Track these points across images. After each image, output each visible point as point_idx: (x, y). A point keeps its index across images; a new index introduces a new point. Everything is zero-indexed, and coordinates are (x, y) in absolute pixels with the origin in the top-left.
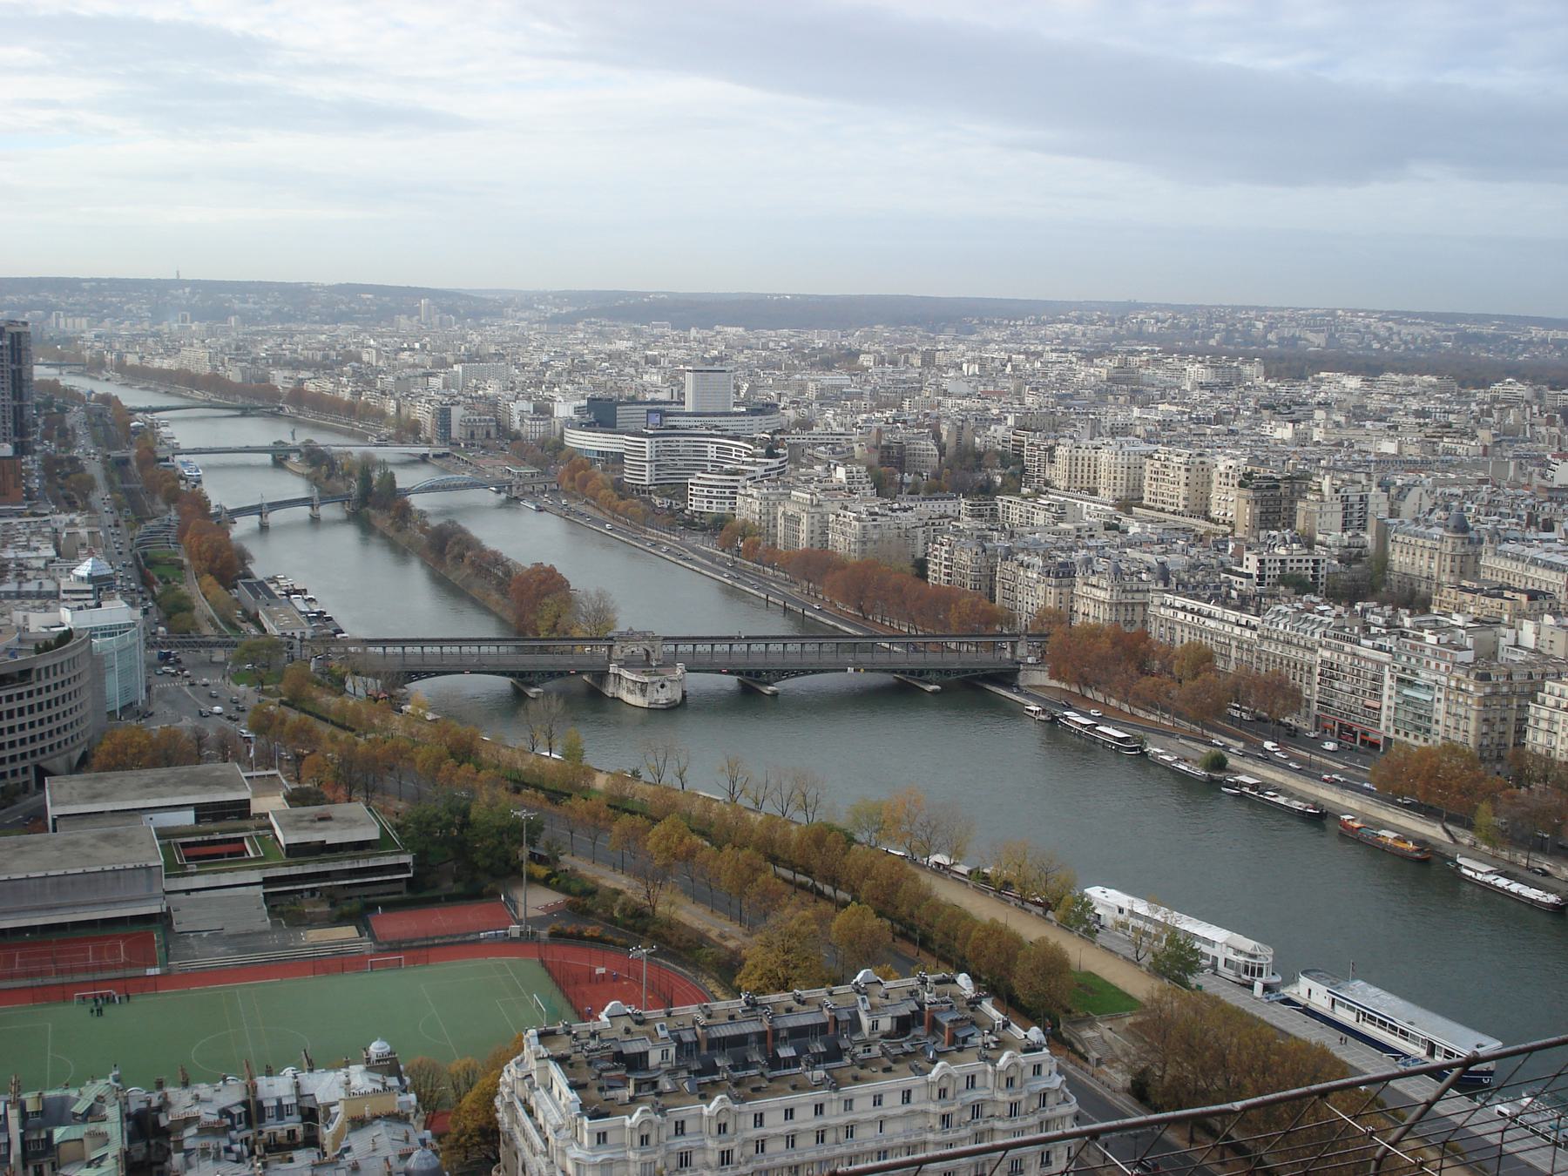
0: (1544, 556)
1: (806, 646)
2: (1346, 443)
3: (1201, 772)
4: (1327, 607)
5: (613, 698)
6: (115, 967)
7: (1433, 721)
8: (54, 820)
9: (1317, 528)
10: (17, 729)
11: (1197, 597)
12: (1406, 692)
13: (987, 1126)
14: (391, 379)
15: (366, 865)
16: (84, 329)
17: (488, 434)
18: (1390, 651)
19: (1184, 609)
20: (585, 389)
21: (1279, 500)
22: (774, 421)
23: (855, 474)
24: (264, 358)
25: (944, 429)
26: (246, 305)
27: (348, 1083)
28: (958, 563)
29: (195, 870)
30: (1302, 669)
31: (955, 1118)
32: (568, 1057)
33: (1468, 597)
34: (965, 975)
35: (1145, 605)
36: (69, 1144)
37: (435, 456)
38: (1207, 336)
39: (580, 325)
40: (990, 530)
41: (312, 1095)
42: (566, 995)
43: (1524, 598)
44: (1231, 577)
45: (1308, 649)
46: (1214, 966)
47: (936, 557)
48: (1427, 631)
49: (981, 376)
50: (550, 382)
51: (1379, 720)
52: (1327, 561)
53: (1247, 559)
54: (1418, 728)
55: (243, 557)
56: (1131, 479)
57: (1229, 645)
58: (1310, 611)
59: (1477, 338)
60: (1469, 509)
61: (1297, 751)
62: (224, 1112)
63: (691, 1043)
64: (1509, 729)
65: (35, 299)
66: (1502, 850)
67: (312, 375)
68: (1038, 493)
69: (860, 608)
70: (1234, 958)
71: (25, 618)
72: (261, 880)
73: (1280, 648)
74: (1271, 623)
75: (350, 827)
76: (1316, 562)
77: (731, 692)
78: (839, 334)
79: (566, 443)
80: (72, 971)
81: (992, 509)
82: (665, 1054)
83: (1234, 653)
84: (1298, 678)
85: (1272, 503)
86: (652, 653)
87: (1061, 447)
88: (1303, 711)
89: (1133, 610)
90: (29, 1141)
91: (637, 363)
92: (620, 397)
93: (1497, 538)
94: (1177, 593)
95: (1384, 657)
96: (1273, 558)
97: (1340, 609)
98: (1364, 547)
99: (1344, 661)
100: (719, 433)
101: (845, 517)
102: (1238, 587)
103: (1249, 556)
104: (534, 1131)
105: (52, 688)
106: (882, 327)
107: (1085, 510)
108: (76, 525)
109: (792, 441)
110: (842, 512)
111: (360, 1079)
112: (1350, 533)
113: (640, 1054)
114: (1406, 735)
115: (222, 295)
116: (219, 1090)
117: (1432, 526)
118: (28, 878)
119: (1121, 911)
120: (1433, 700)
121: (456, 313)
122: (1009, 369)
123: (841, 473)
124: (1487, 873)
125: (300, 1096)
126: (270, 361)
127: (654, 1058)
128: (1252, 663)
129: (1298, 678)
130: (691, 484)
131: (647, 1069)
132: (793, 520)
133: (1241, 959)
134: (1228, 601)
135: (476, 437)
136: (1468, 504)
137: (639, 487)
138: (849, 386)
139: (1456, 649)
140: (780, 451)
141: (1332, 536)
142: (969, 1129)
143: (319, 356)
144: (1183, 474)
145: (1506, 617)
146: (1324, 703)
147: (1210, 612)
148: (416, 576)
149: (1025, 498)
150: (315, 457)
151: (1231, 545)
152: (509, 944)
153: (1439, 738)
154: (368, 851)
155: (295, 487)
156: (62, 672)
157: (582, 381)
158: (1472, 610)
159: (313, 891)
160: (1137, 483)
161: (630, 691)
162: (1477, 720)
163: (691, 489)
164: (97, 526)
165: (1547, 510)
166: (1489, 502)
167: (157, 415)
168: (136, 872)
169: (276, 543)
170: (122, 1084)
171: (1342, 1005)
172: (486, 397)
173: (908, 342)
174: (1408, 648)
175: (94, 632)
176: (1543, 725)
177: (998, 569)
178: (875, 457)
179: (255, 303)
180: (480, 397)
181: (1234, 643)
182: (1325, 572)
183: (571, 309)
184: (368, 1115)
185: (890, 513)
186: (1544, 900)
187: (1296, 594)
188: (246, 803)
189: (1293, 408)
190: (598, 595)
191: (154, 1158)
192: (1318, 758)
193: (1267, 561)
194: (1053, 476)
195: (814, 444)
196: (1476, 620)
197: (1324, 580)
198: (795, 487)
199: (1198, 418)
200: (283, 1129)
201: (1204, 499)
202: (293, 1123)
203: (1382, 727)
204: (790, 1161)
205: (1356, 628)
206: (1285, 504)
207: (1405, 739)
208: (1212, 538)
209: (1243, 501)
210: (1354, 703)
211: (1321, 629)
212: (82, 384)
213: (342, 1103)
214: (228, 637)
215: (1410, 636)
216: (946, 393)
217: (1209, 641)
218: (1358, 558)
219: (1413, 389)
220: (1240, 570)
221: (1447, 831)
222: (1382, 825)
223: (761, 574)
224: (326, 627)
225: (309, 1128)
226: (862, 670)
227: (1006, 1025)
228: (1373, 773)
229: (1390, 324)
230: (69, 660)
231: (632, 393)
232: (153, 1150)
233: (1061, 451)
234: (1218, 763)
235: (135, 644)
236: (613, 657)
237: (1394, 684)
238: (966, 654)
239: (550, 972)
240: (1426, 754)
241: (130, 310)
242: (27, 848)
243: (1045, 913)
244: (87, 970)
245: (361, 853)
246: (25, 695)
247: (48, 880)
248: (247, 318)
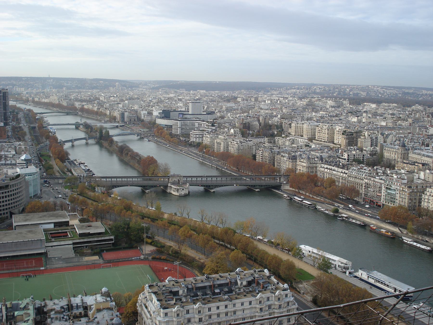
0: (426, 154)
1: (223, 178)
2: (372, 123)
3: (332, 213)
4: (366, 168)
5: (169, 193)
6: (32, 267)
7: (396, 199)
8: (15, 227)
9: (364, 146)
10: (5, 201)
11: (331, 165)
12: (388, 191)
13: (273, 311)
14: (108, 105)
15: (101, 239)
16: (23, 91)
17: (135, 120)
18: (384, 180)
19: (327, 168)
20: (161, 107)
21: (353, 138)
22: (214, 116)
23: (236, 131)
24: (73, 99)
25: (261, 119)
26: (68, 84)
27: (96, 299)
28: (265, 156)
29: (54, 240)
30: (359, 185)
31: (264, 309)
32: (157, 292)
33: (405, 165)
34: (266, 269)
35: (316, 167)
36: (19, 316)
38: (333, 93)
39: (160, 90)
40: (273, 146)
41: (86, 303)
42: (156, 275)
43: (421, 165)
44: (340, 159)
45: (361, 179)
46: (335, 267)
47: (258, 154)
48: (394, 174)
49: (271, 104)
50: (152, 106)
51: (381, 199)
52: (367, 155)
53: (344, 155)
54: (392, 201)
55: (67, 154)
56: (312, 132)
57: (340, 178)
58: (362, 169)
59: (408, 93)
60: (406, 141)
61: (358, 208)
62: (62, 307)
63: (191, 288)
64: (417, 201)
65: (10, 83)
66: (415, 235)
67: (86, 104)
68: (287, 136)
69: (237, 168)
70: (341, 265)
71: (7, 171)
72: (72, 243)
73: (353, 179)
74: (351, 172)
75: (97, 229)
76: (363, 155)
78: (232, 92)
79: (156, 122)
80: (20, 268)
81: (274, 141)
82: (184, 291)
83: (341, 181)
84: (358, 187)
85: (351, 139)
86: (180, 180)
87: (293, 124)
88: (360, 197)
89: (313, 169)
90: (8, 315)
91: (176, 100)
92: (171, 110)
93: (413, 149)
94: (325, 164)
95: (382, 182)
96: (351, 154)
97: (370, 168)
98: (377, 151)
99: (371, 183)
100: (199, 120)
101: (233, 143)
102: (342, 162)
103: (345, 154)
104: (147, 312)
105: (14, 190)
106: (243, 90)
107: (300, 141)
108: (21, 145)
109: (219, 122)
110: (232, 142)
111: (99, 298)
112: (373, 147)
113: (177, 291)
114: (388, 203)
116: (61, 301)
117: (395, 145)
118: (8, 243)
119: (310, 252)
120: (396, 193)
121: (126, 86)
122: (279, 102)
123: (232, 131)
124: (411, 241)
125: (83, 303)
126: (75, 100)
127: (181, 292)
128: (346, 183)
129: (358, 187)
130: (191, 134)
131: (179, 295)
132: (219, 144)
133: (343, 265)
134: (339, 166)
135: (131, 121)
136: (406, 139)
137: (176, 135)
138: (235, 107)
139: (402, 179)
140: (216, 125)
141: (368, 148)
142: (267, 312)
143: (88, 98)
144: (327, 131)
145: (416, 171)
146: (366, 194)
147: (334, 169)
148: (115, 159)
149: (283, 138)
151: (340, 151)
152: (140, 261)
153: (397, 204)
154: (102, 235)
155: (82, 135)
156: (17, 186)
157: (161, 105)
158: (406, 168)
159: (86, 246)
160: (314, 133)
161: (174, 191)
162: (408, 199)
163: (191, 135)
164: (27, 145)
165: (427, 141)
166: (411, 139)
167: (43, 115)
168: (38, 241)
169: (76, 150)
170: (34, 299)
171: (371, 278)
172: (134, 110)
173: (251, 94)
174: (389, 179)
175: (26, 175)
176: (426, 200)
177: (276, 157)
178: (242, 126)
179: (70, 84)
180: (133, 110)
181: (341, 178)
182: (366, 158)
183: (158, 85)
184: (102, 308)
185: (246, 142)
186: (426, 249)
188: (68, 222)
189: (357, 113)
190: (165, 164)
191: (42, 320)
192: (364, 210)
193: (350, 155)
194: (291, 132)
195: (225, 123)
196: (407, 171)
197: (366, 160)
198: (219, 135)
200: (78, 312)
201: (333, 138)
202: (81, 310)
203: (382, 201)
204: (218, 321)
205: (375, 174)
206: (355, 139)
207: (388, 204)
208: (335, 149)
209: (343, 139)
210: (374, 194)
211: (365, 174)
212: (23, 106)
213: (94, 305)
214: (63, 176)
215: (389, 176)
216: (261, 109)
217: (334, 177)
218: (375, 154)
219: (390, 108)
220: (342, 157)
221: (400, 230)
222: (382, 228)
223: (210, 159)
224: (90, 173)
225: (85, 312)
226: (238, 185)
227: (278, 283)
228: (379, 214)
229: (384, 89)
230: (19, 183)
231: (175, 109)
232: (42, 318)
233: (293, 125)
234: (336, 211)
235: (37, 178)
236: (169, 181)
237: (385, 189)
238: (267, 181)
239: (152, 269)
240: (394, 208)
241: (36, 86)
242: (7, 234)
243: (289, 252)
244: (24, 268)
245: (100, 236)
246: (7, 192)
247: (13, 243)
248: (68, 88)
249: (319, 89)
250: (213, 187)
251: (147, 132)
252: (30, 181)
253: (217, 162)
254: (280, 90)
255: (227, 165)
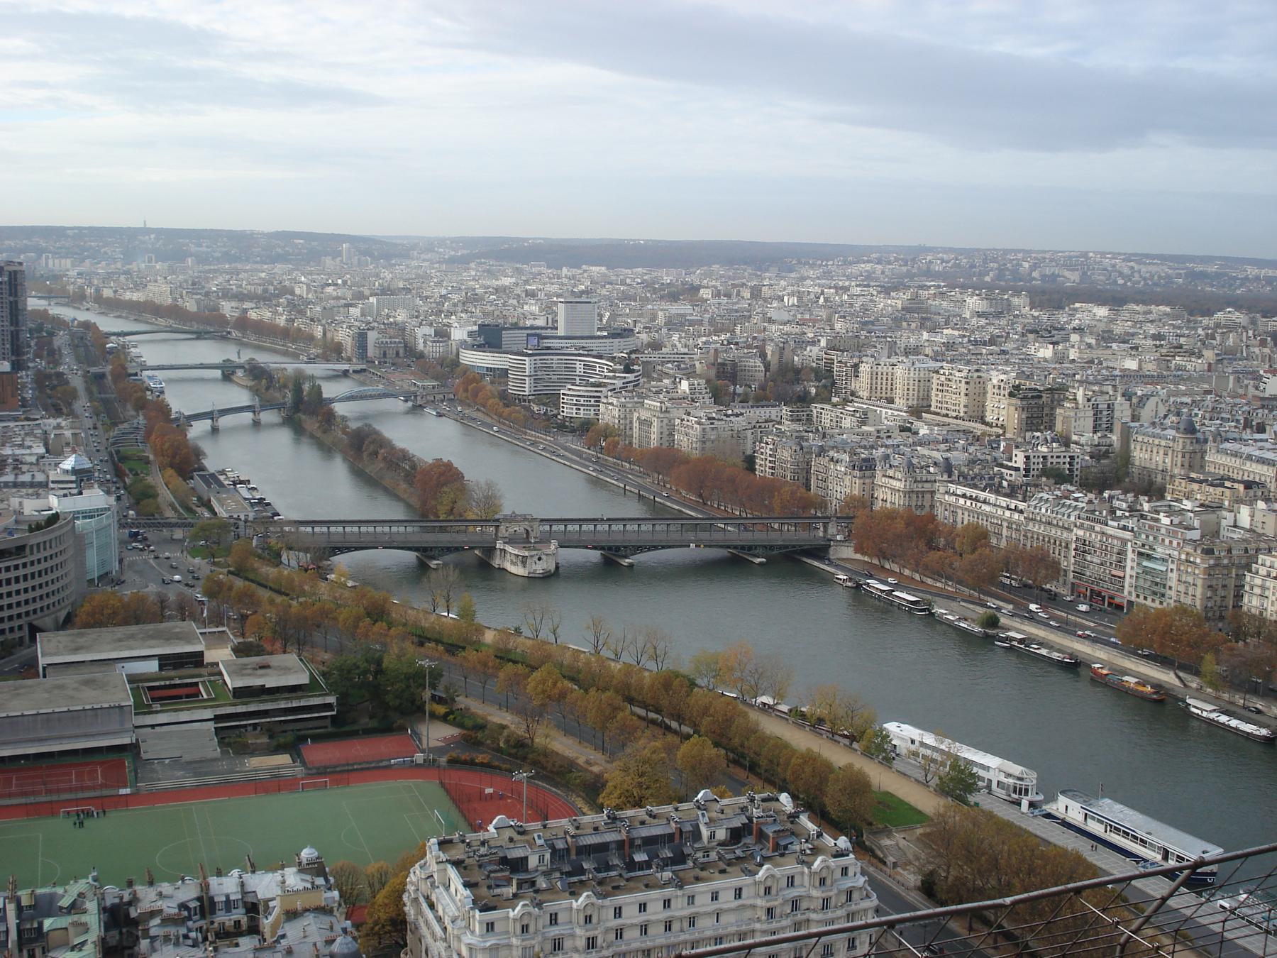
0: (1257, 453)
1: (657, 526)
2: (1096, 361)
3: (978, 629)
4: (1080, 495)
5: (499, 568)
6: (94, 788)
7: (1167, 587)
8: (44, 668)
9: (1073, 430)
10: (14, 594)
11: (975, 487)
12: (1145, 563)
13: (804, 917)
14: (318, 309)
15: (298, 705)
16: (69, 268)
17: (397, 353)
18: (1132, 531)
19: (964, 496)
20: (476, 317)
21: (1042, 407)
22: (630, 343)
23: (696, 386)
24: (215, 292)
25: (769, 350)
26: (200, 249)
27: (284, 882)
29: (159, 709)
30: (1060, 545)
31: (778, 911)
32: (463, 861)
33: (1195, 486)
35: (933, 493)
36: (56, 932)
37: (355, 372)
38: (983, 274)
39: (472, 265)
41: (254, 892)
42: (461, 811)
43: (1241, 487)
44: (1003, 470)
45: (1066, 528)
47: (762, 453)
48: (1162, 514)
50: (448, 311)
51: (1123, 586)
52: (1081, 457)
53: (1016, 455)
54: (1155, 593)
55: (198, 454)
56: (921, 390)
57: (1001, 525)
58: (1067, 498)
59: (1203, 275)
60: (1196, 415)
61: (1056, 612)
62: (183, 906)
63: (563, 850)
64: (1229, 594)
65: (29, 243)
66: (1223, 693)
67: (254, 306)
68: (846, 401)
69: (700, 496)
70: (1005, 780)
71: (21, 503)
72: (213, 717)
73: (1042, 528)
74: (1035, 508)
75: (285, 674)
76: (1072, 458)
77: (595, 564)
78: (684, 272)
79: (461, 361)
80: (59, 791)
81: (808, 415)
82: (541, 859)
83: (1005, 532)
84: (1057, 553)
85: (1036, 410)
86: (531, 532)
87: (864, 364)
88: (1061, 579)
89: (923, 497)
90: (24, 930)
91: (519, 296)
92: (505, 323)
93: (1219, 438)
94: (959, 483)
95: (1127, 535)
96: (1037, 455)
97: (1091, 496)
98: (1111, 445)
99: (1095, 538)
100: (586, 353)
101: (688, 421)
102: (1008, 478)
103: (1017, 453)
104: (435, 921)
105: (43, 560)
106: (718, 266)
107: (883, 416)
108: (62, 428)
109: (645, 359)
110: (685, 417)
112: (1099, 434)
113: (521, 858)
114: (1145, 598)
115: (181, 240)
116: (178, 888)
117: (1166, 429)
118: (23, 715)
119: (913, 742)
120: (1167, 570)
121: (371, 255)
122: (821, 301)
123: (685, 386)
124: (1211, 711)
125: (244, 893)
126: (220, 294)
127: (533, 862)
128: (1019, 540)
129: (1057, 553)
130: (563, 394)
131: (527, 871)
132: (646, 424)
133: (1011, 781)
134: (1000, 489)
135: (388, 356)
136: (1196, 411)
137: (520, 397)
138: (692, 315)
139: (1186, 528)
140: (636, 367)
141: (1085, 437)
142: (789, 920)
143: (260, 290)
145: (1226, 503)
146: (1078, 573)
147: (986, 499)
148: (339, 470)
149: (835, 405)
150: (256, 373)
151: (1003, 444)
152: (414, 769)
153: (1172, 602)
154: (300, 694)
155: (241, 397)
156: (51, 547)
157: (474, 310)
158: (1198, 497)
159: (255, 726)
160: (926, 393)
161: (513, 563)
162: (1203, 586)
163: (563, 399)
164: (79, 429)
165: (1260, 415)
166: (1213, 409)
167: (128, 338)
168: (111, 711)
169: (225, 442)
170: (99, 883)
171: (1093, 818)
172: (396, 323)
173: (739, 278)
174: (1147, 528)
175: (76, 515)
176: (1257, 591)
177: (813, 464)
178: (713, 373)
179: (207, 247)
180: (391, 323)
181: (1005, 524)
182: (1079, 466)
183: (465, 252)
184: (299, 908)
185: (725, 418)
186: (1258, 733)
187: (1055, 484)
188: (200, 654)
189: (1053, 332)
190: (487, 484)
191: (125, 944)
192: (1073, 618)
193: (1032, 457)
195: (663, 362)
196: (1202, 505)
197: (1078, 473)
198: (647, 397)
199: (976, 341)
200: (230, 920)
201: (981, 406)
202: (239, 915)
203: (1126, 593)
204: (643, 946)
205: (1105, 512)
206: (1046, 411)
207: (1144, 602)
208: (987, 438)
209: (1013, 408)
210: (1102, 573)
211: (1076, 513)
212: (67, 313)
213: (278, 898)
214: (185, 519)
215: (1149, 518)
216: (770, 320)
217: (985, 522)
218: (1106, 455)
219: (1151, 317)
220: (1010, 464)
221: (1179, 677)
222: (1126, 672)
223: (620, 468)
224: (266, 511)
225: (252, 919)
226: (702, 546)
227: (819, 835)
228: (1118, 630)
229: (1132, 264)
230: (56, 538)
231: (515, 320)
232: (125, 937)
233: (864, 368)
234: (992, 622)
235: (110, 525)
236: (500, 535)
237: (1135, 557)
238: (786, 533)
239: (448, 792)
240: (1161, 614)
241: (106, 253)
242: (22, 691)
243: (851, 744)
244: (70, 790)
245: (294, 695)
246: (21, 566)
247: (39, 717)
248: (201, 259)
249: (942, 263)
250: (628, 551)
251: (434, 388)
252: (90, 535)
253: (641, 477)
254: (827, 265)
255: (668, 486)
